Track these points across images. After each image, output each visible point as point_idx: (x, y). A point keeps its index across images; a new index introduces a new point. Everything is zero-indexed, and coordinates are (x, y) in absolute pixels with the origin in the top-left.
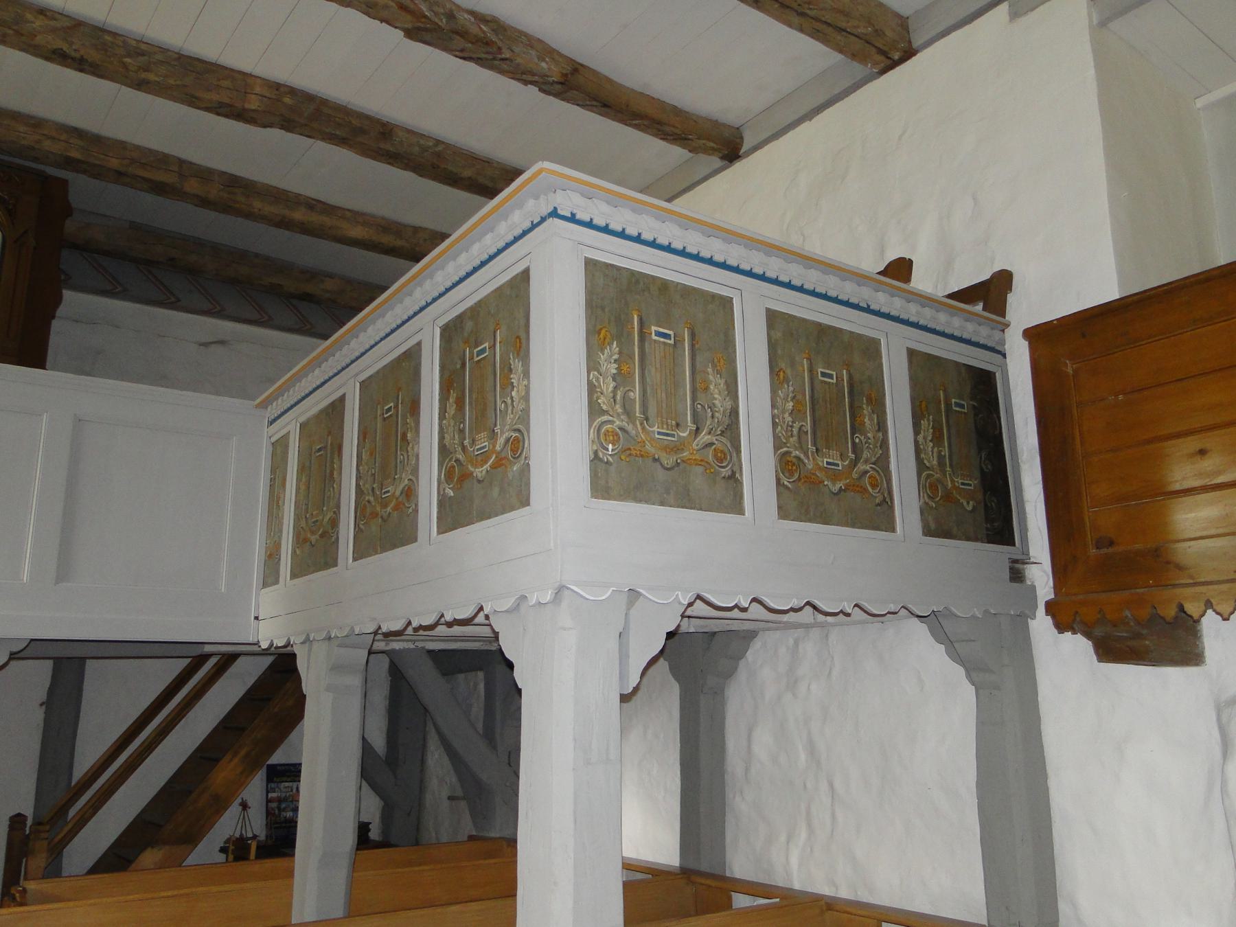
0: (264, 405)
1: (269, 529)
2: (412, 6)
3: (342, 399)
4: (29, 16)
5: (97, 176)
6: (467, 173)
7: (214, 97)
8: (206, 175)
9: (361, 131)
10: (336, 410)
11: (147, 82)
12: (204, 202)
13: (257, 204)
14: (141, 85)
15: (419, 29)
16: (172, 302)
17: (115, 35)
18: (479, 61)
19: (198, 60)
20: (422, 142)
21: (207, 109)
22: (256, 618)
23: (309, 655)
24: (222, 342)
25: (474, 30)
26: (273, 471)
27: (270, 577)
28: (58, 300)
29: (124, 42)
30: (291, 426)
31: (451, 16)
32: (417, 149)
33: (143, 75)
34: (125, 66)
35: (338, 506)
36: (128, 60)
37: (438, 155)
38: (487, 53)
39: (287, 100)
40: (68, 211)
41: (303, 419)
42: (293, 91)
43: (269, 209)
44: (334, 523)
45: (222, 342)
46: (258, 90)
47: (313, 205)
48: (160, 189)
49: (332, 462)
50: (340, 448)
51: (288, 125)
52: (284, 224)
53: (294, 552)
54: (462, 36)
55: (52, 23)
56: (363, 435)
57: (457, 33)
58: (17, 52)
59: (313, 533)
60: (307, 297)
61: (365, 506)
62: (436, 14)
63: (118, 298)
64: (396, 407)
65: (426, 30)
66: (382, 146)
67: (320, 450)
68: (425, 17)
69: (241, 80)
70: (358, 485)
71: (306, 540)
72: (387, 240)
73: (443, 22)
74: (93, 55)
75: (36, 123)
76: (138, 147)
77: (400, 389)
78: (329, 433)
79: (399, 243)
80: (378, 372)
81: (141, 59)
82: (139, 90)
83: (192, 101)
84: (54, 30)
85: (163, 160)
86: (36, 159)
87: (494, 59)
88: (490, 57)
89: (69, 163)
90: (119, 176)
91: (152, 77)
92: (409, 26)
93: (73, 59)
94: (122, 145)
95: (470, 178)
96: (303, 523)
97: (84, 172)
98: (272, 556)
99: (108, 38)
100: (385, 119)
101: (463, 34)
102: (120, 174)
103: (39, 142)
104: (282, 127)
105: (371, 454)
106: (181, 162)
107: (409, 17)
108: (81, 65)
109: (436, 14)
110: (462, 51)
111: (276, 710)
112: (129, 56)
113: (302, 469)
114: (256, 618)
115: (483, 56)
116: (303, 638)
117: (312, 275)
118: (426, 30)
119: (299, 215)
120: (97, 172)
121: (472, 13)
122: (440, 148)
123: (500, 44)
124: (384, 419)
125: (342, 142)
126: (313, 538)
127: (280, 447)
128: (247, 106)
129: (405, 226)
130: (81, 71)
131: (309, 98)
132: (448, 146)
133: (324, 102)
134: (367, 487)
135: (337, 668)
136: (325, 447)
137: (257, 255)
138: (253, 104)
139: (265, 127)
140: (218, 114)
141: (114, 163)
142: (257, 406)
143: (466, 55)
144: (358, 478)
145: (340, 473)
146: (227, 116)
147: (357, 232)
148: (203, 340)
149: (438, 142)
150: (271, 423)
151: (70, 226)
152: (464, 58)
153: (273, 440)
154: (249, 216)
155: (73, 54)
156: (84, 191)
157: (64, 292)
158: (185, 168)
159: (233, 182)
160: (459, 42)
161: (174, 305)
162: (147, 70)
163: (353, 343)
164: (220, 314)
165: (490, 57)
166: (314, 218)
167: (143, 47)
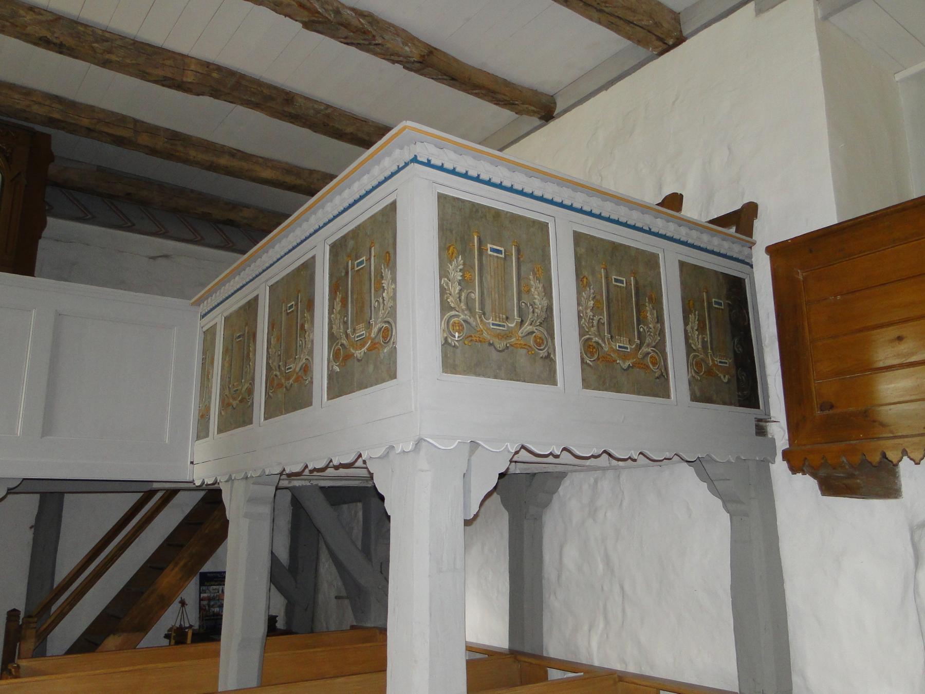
0: (198, 303)
1: (201, 396)
4: (22, 12)
5: (72, 132)
6: (349, 130)
7: (160, 72)
9: (271, 98)
10: (251, 307)
12: (153, 152)
13: (192, 153)
14: (105, 64)
15: (313, 22)
16: (128, 226)
17: (86, 26)
18: (358, 46)
20: (316, 106)
21: (156, 82)
22: (192, 463)
23: (231, 491)
24: (166, 256)
25: (355, 22)
26: (204, 353)
27: (202, 432)
28: (43, 225)
29: (93, 31)
30: (217, 319)
31: (337, 12)
32: (312, 111)
33: (107, 56)
34: (94, 49)
35: (253, 379)
36: (96, 45)
38: (365, 40)
39: (215, 75)
40: (51, 158)
42: (219, 68)
43: (201, 157)
44: (250, 391)
45: (166, 256)
46: (193, 67)
47: (234, 153)
48: (119, 141)
49: (249, 346)
51: (215, 93)
52: (212, 167)
53: (220, 413)
54: (346, 27)
55: (39, 17)
56: (272, 325)
57: (342, 24)
58: (13, 39)
59: (234, 399)
60: (230, 223)
61: (273, 379)
62: (326, 10)
64: (297, 304)
65: (319, 22)
67: (239, 337)
68: (318, 12)
69: (181, 60)
70: (268, 363)
71: (229, 404)
72: (290, 179)
73: (331, 17)
74: (70, 41)
75: (27, 92)
76: (103, 110)
77: (299, 291)
78: (247, 324)
79: (298, 182)
80: (283, 279)
81: (105, 44)
82: (104, 67)
83: (144, 76)
84: (40, 23)
85: (122, 120)
86: (27, 119)
87: (370, 44)
88: (367, 42)
89: (51, 122)
90: (89, 132)
91: (113, 57)
92: (306, 19)
93: (55, 44)
94: (92, 108)
95: (352, 133)
96: (227, 392)
97: (63, 129)
98: (204, 416)
99: (81, 28)
100: (288, 89)
101: (346, 25)
102: (90, 130)
103: (29, 106)
105: (278, 340)
106: (136, 121)
107: (306, 13)
109: (326, 10)
110: (346, 38)
112: (97, 42)
113: (226, 351)
114: (192, 463)
115: (362, 42)
117: (234, 206)
118: (319, 22)
119: (224, 161)
120: (74, 129)
121: (353, 9)
122: (329, 111)
123: (374, 33)
124: (288, 314)
125: (256, 106)
126: (235, 403)
127: (209, 335)
128: (185, 79)
129: (304, 169)
130: (61, 53)
131: (231, 73)
132: (335, 109)
133: (243, 76)
135: (252, 500)
136: (244, 335)
137: (192, 191)
138: (190, 78)
141: (85, 122)
143: (349, 41)
145: (255, 354)
146: (170, 87)
147: (267, 174)
148: (152, 255)
149: (328, 106)
150: (203, 316)
151: (53, 169)
152: (347, 44)
153: (205, 329)
154: (186, 161)
155: (55, 40)
156: (63, 143)
157: (48, 218)
158: (138, 126)
159: (175, 136)
160: (343, 32)
162: (110, 52)
164: (165, 235)
165: (367, 42)
166: (236, 164)
167: (107, 35)
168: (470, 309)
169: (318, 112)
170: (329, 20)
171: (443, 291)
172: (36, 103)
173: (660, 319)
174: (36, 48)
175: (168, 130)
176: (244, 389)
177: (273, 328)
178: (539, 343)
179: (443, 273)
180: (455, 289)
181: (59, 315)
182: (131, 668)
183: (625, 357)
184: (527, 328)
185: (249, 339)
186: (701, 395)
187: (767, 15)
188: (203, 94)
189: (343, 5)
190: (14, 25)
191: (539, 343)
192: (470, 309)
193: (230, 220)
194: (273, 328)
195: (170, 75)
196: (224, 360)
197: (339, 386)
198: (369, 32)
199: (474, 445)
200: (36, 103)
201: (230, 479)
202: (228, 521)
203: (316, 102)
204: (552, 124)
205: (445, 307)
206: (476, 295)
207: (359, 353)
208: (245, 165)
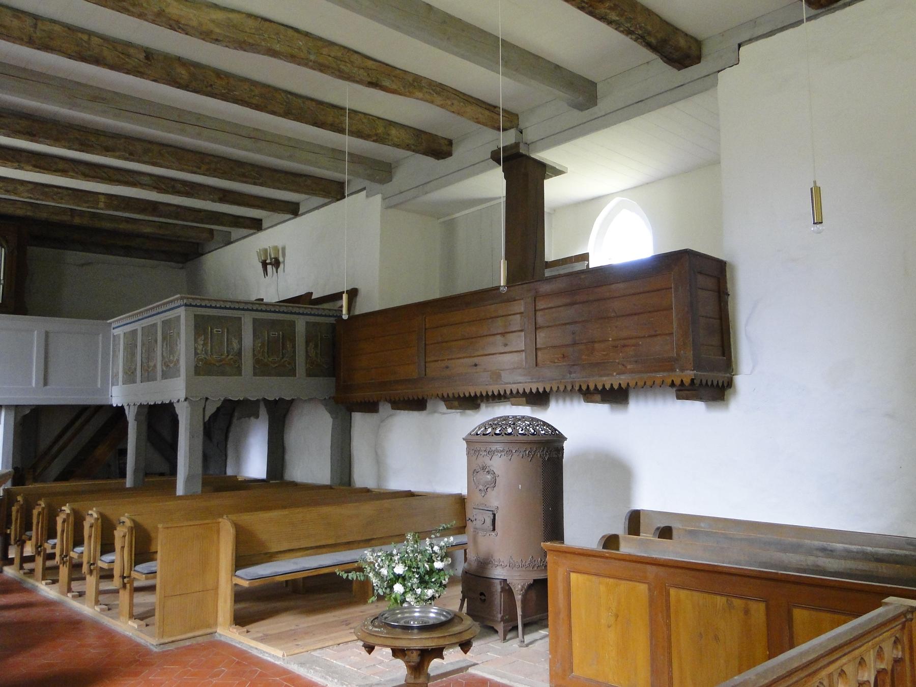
44: (135, 369)
168: (206, 353)
171: (196, 349)
173: (294, 347)
178: (235, 362)
179: (196, 341)
180: (200, 347)
181: (47, 334)
182: (201, 522)
183: (275, 363)
184: (230, 357)
186: (310, 374)
187: (371, 199)
191: (235, 362)
192: (206, 353)
197: (165, 376)
199: (207, 399)
202: (582, 110)
204: (298, 219)
205: (196, 354)
206: (209, 348)
207: (171, 365)
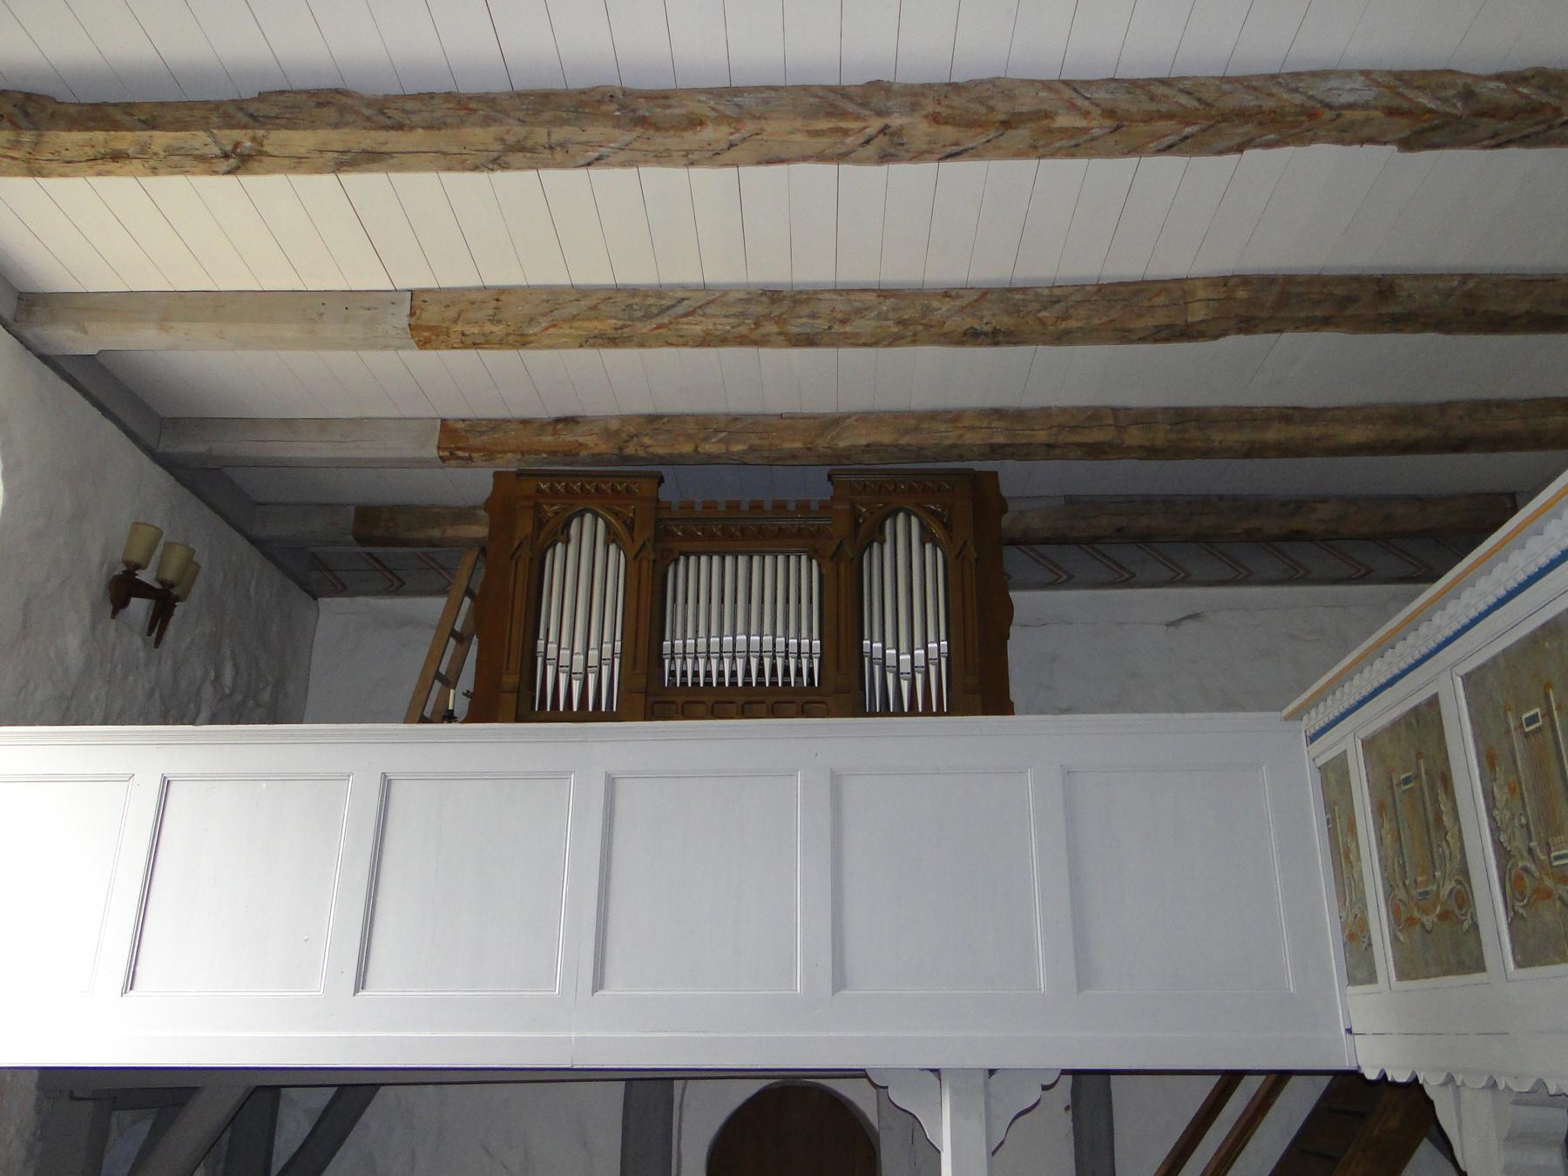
0: (1297, 715)
1: (1341, 898)
2: (1405, 105)
3: (1434, 702)
4: (935, 304)
5: (1026, 457)
6: (1523, 306)
7: (1149, 322)
8: (1145, 418)
9: (1350, 300)
10: (1426, 717)
11: (1068, 332)
12: (1151, 453)
13: (1217, 437)
14: (1062, 338)
15: (1423, 131)
16: (1126, 579)
17: (1024, 290)
18: (1526, 141)
19: (1120, 284)
20: (1441, 285)
21: (1142, 340)
22: (1349, 1031)
23: (1458, 1110)
24: (1193, 616)
25: (1509, 99)
26: (1329, 807)
27: (1361, 970)
28: (1009, 608)
29: (1036, 295)
30: (1347, 741)
31: (1468, 94)
32: (1436, 297)
33: (1063, 325)
34: (1042, 322)
35: (1464, 871)
36: (1043, 314)
37: (1470, 295)
38: (1538, 123)
39: (1241, 294)
40: (1002, 505)
41: (1366, 732)
42: (1245, 280)
43: (1234, 438)
44: (1463, 898)
45: (1193, 616)
46: (1201, 294)
47: (1286, 415)
48: (1096, 451)
49: (1436, 802)
50: (1446, 779)
51: (1247, 325)
52: (1253, 451)
53: (1395, 940)
54: (1493, 116)
55: (958, 303)
56: (1489, 760)
57: (1483, 114)
58: (928, 348)
59: (1424, 911)
60: (1297, 536)
61: (1519, 878)
62: (1444, 100)
63: (1067, 588)
64: (1548, 714)
65: (1434, 128)
66: (1383, 310)
67: (1407, 781)
68: (1430, 111)
69: (1177, 289)
70: (1497, 844)
71: (1411, 921)
72: (1402, 433)
73: (1459, 108)
74: (1006, 322)
75: (954, 417)
76: (1064, 410)
77: (1548, 685)
78: (1419, 755)
79: (1422, 433)
80: (1494, 659)
81: (1057, 307)
82: (1061, 344)
83: (1124, 336)
84: (962, 309)
85: (1094, 416)
86: (961, 458)
87: (1551, 127)
88: (1544, 127)
89: (995, 451)
90: (1050, 450)
91: (1073, 324)
92: (1406, 133)
93: (986, 334)
94: (1046, 412)
95: (1527, 313)
96: (1401, 893)
97: (1012, 456)
98: (1356, 937)
99: (1018, 296)
100: (1378, 272)
101: (1492, 111)
102: (1050, 446)
103: (960, 437)
104: (1240, 331)
105: (1512, 791)
106: (1115, 411)
107: (1404, 121)
108: (995, 337)
109: (1444, 100)
110: (1495, 135)
111: (1375, 1133)
112: (1044, 308)
113: (1380, 809)
114: (1349, 1031)
115: (1531, 130)
116: (1442, 1079)
117: (1298, 505)
118: (1434, 128)
119: (1272, 435)
120: (1022, 452)
121: (1499, 77)
122: (1471, 284)
123: (1556, 103)
124: (1526, 735)
125: (1326, 323)
126: (1428, 920)
127: (1334, 776)
128: (1190, 319)
129: (1427, 406)
130: (996, 344)
131: (1268, 281)
132: (1482, 278)
133: (1290, 280)
134: (1518, 844)
135: (1517, 1138)
136: (1418, 777)
137: (1221, 498)
138: (1198, 313)
139: (1216, 337)
140: (1156, 341)
141: (1042, 436)
142: (1286, 718)
143: (1501, 139)
144: (1495, 830)
145: (1457, 819)
146: (1167, 340)
147: (1357, 434)
148: (1173, 618)
149: (1465, 278)
150: (1313, 738)
151: (1006, 520)
152: (1498, 146)
153: (1321, 761)
154: (1206, 453)
155: (987, 328)
156: (1014, 478)
157: (1013, 595)
158: (1121, 417)
159: (1181, 417)
160: (1488, 126)
161: (1129, 582)
162: (1065, 317)
163: (1438, 618)
164: (1185, 580)
165: (1544, 127)
166: (1296, 432)
167: (1057, 292)
169: (1449, 293)
170: (1454, 116)
172: (972, 428)
174: (499, 176)
175: (1166, 409)
176: (1444, 892)
177: (1492, 765)
185: (1433, 787)
188: (1224, 333)
189: (1477, 77)
190: (927, 326)
193: (1298, 532)
194: (1492, 765)
195: (1166, 321)
196: (1378, 826)
198: (1543, 105)
200: (972, 428)
201: (1450, 1079)
203: (1439, 277)
208: (1315, 431)
